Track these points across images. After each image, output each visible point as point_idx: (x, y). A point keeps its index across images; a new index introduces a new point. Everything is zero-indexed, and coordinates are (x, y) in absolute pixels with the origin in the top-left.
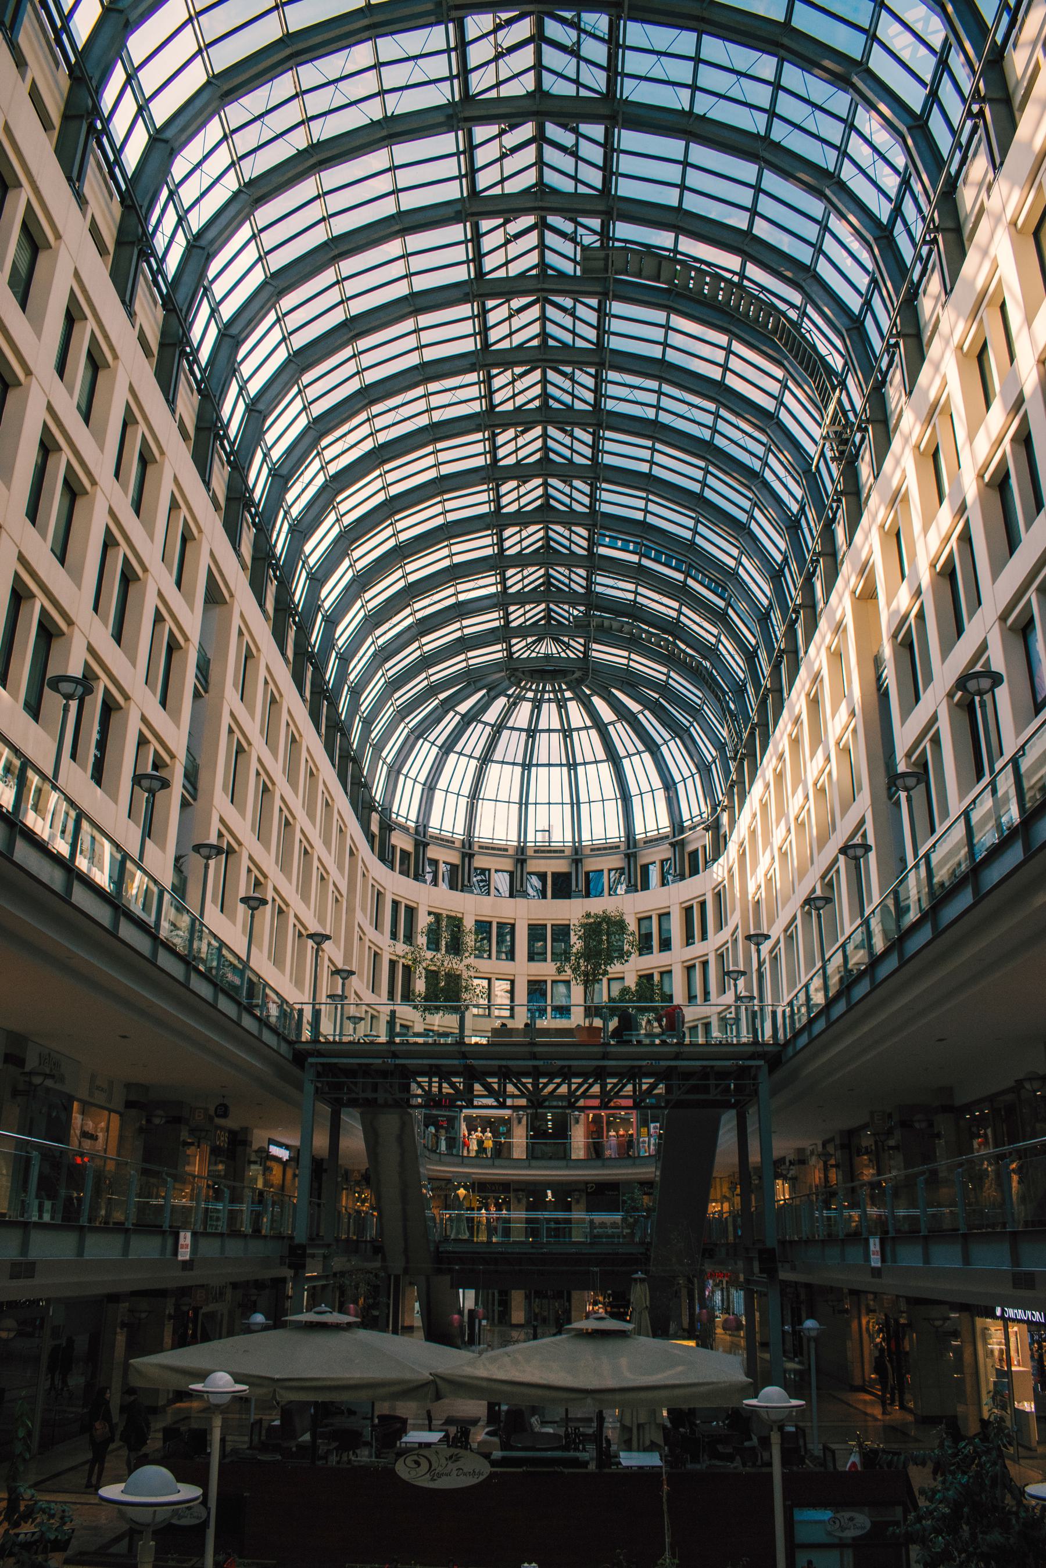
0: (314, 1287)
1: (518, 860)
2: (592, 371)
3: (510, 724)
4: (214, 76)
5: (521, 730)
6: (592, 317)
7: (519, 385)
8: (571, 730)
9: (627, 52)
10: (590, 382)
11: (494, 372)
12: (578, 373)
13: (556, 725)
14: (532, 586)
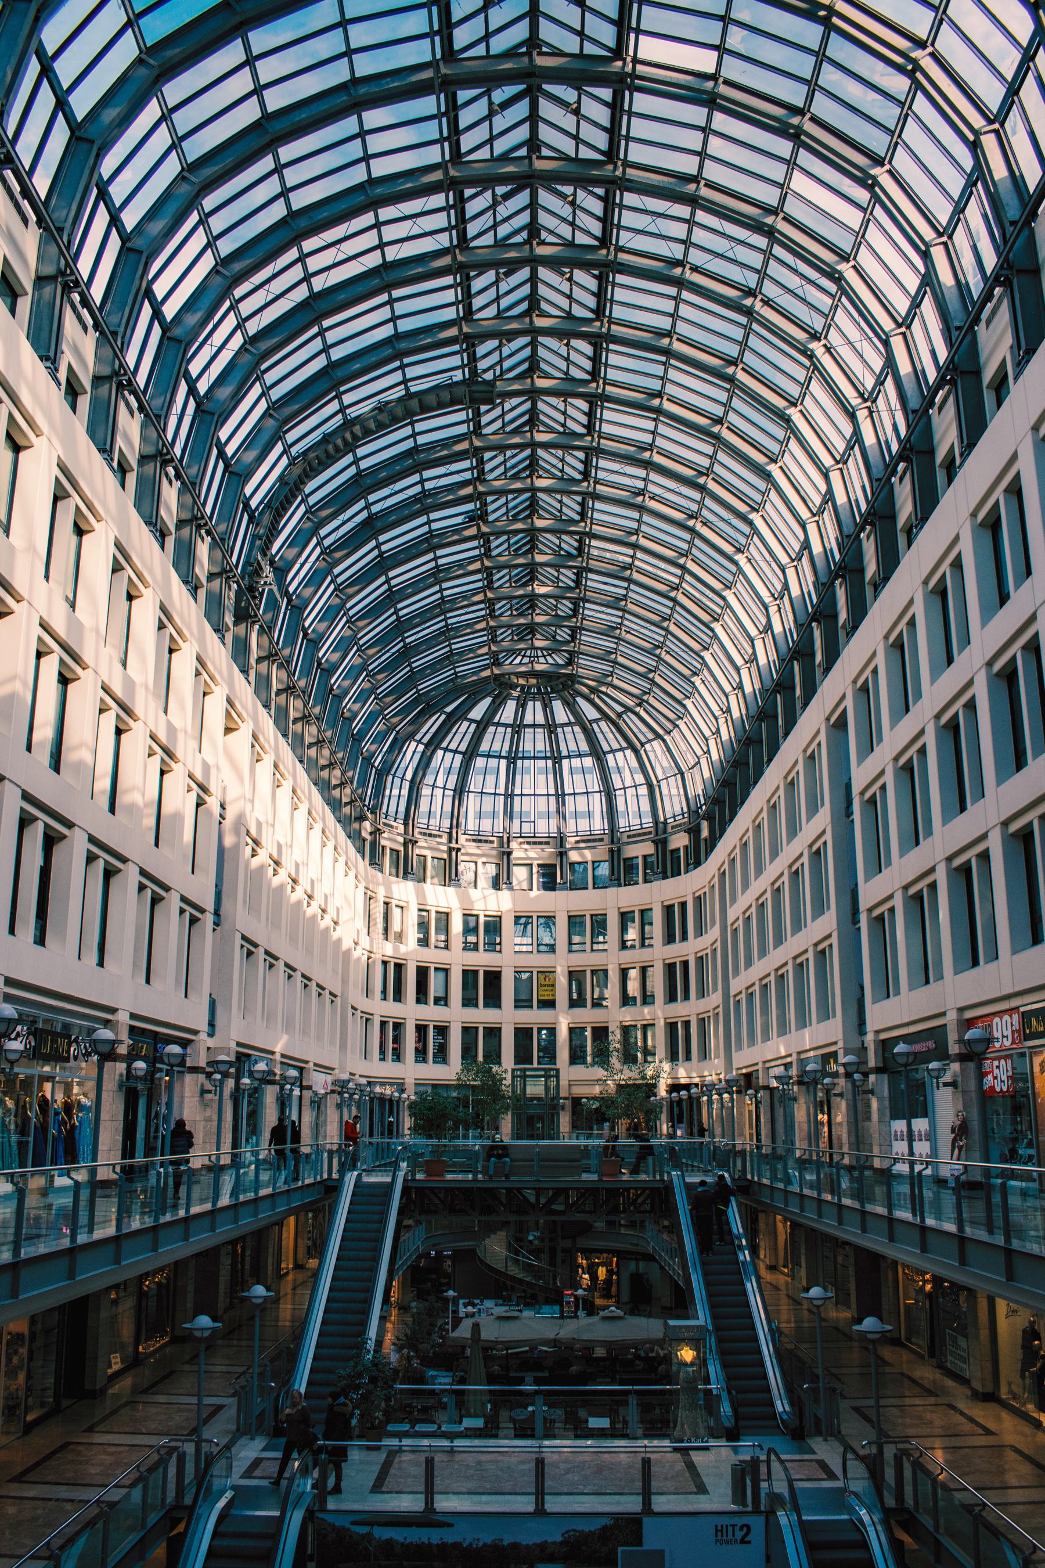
0: (555, 1222)
1: (504, 853)
2: (600, 191)
3: (496, 720)
4: (222, 260)
5: (507, 725)
6: (603, 115)
7: (503, 211)
8: (556, 726)
9: (635, 94)
10: (597, 208)
11: (468, 192)
12: (581, 194)
13: (540, 719)
14: (516, 470)
